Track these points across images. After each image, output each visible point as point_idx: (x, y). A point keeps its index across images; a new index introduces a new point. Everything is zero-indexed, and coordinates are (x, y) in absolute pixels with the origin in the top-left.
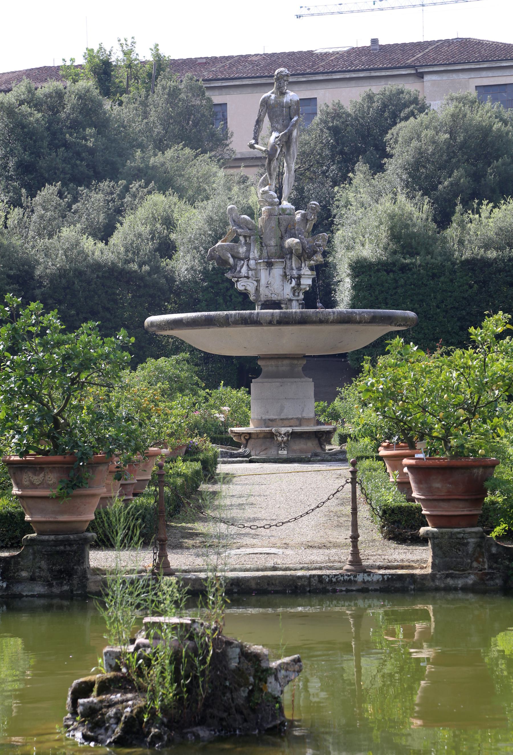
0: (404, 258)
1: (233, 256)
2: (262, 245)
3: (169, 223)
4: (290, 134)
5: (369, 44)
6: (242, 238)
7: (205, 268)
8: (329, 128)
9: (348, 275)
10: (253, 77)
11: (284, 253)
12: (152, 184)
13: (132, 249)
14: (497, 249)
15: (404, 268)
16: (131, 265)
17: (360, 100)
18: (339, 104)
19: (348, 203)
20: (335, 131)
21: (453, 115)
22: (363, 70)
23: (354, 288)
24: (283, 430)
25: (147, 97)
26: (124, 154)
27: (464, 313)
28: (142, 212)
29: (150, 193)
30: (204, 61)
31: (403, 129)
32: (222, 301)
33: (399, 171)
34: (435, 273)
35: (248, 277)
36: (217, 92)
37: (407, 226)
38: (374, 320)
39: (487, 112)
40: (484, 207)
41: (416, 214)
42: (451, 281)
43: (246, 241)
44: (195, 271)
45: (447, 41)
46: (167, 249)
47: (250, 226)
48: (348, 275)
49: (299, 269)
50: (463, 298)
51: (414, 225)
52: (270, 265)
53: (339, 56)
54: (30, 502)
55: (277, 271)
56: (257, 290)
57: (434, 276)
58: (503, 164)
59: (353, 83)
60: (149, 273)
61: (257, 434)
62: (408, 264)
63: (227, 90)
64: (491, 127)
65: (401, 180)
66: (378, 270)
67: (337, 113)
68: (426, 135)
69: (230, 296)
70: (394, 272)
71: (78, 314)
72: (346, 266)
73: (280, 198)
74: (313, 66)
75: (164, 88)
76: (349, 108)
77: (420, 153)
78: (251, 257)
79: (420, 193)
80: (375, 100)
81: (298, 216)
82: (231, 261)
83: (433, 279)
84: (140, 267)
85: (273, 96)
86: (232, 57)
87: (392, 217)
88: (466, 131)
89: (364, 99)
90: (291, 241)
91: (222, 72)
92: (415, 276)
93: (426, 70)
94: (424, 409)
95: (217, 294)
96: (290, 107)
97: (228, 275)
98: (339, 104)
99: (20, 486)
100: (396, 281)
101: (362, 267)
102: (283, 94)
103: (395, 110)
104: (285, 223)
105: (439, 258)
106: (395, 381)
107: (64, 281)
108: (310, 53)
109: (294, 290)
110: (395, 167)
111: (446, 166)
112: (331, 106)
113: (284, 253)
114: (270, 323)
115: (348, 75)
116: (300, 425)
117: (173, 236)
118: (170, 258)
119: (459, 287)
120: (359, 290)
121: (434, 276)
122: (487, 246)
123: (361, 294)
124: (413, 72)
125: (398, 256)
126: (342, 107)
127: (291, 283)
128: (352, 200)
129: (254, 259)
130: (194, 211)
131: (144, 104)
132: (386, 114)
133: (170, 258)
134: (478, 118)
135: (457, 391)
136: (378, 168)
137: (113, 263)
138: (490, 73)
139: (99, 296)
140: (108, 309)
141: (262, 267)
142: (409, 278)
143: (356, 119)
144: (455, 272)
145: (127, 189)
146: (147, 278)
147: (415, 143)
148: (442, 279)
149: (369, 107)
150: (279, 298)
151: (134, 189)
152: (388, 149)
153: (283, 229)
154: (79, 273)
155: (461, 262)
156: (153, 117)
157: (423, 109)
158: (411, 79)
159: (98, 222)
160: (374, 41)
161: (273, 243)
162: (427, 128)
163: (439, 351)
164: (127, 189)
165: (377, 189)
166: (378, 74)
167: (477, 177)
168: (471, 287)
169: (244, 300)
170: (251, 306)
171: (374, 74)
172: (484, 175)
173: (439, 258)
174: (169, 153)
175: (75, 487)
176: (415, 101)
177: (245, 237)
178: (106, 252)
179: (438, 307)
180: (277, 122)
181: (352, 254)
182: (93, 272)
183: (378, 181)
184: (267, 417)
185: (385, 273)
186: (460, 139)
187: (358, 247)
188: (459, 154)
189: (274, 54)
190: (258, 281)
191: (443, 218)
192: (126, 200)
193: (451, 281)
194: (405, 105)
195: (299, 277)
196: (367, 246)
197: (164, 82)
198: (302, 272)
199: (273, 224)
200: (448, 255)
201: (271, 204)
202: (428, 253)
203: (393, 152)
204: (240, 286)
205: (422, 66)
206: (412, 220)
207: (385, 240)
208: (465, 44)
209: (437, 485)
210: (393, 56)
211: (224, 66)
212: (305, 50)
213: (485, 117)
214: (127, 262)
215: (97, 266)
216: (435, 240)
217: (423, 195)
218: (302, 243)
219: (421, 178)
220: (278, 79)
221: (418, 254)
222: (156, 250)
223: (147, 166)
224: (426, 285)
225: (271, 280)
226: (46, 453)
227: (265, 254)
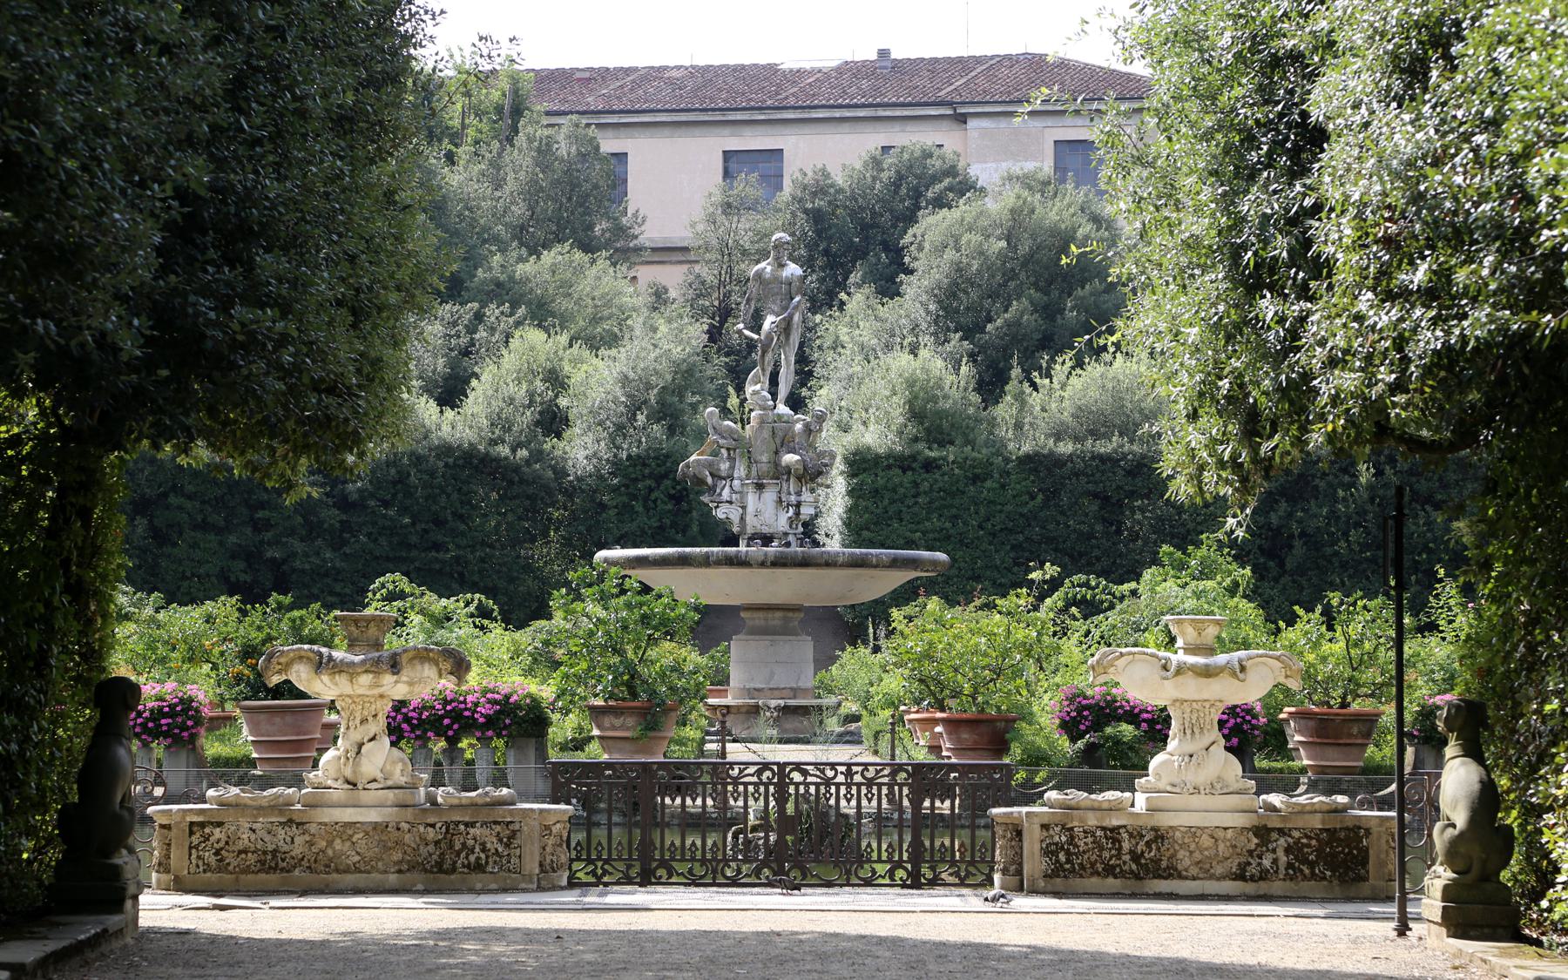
0: (930, 449)
2: (751, 461)
3: (556, 380)
4: (791, 317)
5: (873, 56)
6: (724, 451)
7: (615, 456)
8: (806, 211)
9: (842, 473)
10: (674, 111)
11: (780, 473)
12: (522, 311)
13: (501, 423)
14: (1077, 439)
15: (929, 465)
16: (500, 448)
17: (858, 165)
18: (824, 170)
19: (837, 345)
20: (816, 217)
21: (1012, 211)
22: (864, 106)
23: (850, 493)
24: (773, 703)
25: (500, 155)
26: (473, 260)
27: (1021, 538)
28: (510, 360)
29: (518, 324)
30: (587, 75)
31: (931, 226)
32: (641, 509)
33: (924, 298)
35: (730, 502)
36: (610, 133)
37: (935, 399)
38: (895, 563)
39: (1069, 206)
40: (1058, 367)
41: (950, 378)
42: (1003, 486)
44: (600, 459)
45: (1008, 57)
46: (553, 422)
48: (842, 473)
49: (799, 494)
50: (1022, 515)
51: (946, 397)
52: (760, 487)
53: (824, 77)
54: (610, 742)
55: (770, 496)
56: (742, 519)
57: (976, 479)
58: (1092, 294)
59: (846, 127)
60: (528, 462)
61: (738, 707)
62: (935, 459)
63: (629, 131)
64: (1075, 231)
65: (928, 312)
66: (889, 467)
67: (821, 187)
68: (969, 241)
69: (655, 501)
70: (913, 470)
71: (413, 524)
73: (774, 400)
74: (777, 94)
75: (530, 140)
76: (840, 179)
77: (959, 270)
79: (958, 335)
80: (885, 166)
81: (799, 426)
82: (709, 480)
83: (974, 483)
84: (514, 451)
85: (769, 269)
86: (636, 69)
87: (911, 383)
88: (1033, 236)
89: (866, 164)
90: (790, 458)
91: (619, 98)
93: (971, 110)
94: (956, 670)
95: (634, 497)
97: (705, 499)
98: (824, 170)
99: (599, 727)
100: (916, 484)
101: (864, 460)
102: (782, 266)
103: (919, 187)
105: (984, 451)
106: (931, 644)
107: (393, 471)
108: (772, 69)
109: (791, 521)
110: (917, 292)
111: (999, 294)
112: (810, 174)
113: (780, 473)
114: (762, 564)
115: (837, 114)
116: (795, 697)
117: (563, 402)
118: (559, 436)
121: (976, 479)
122: (1058, 437)
124: (950, 112)
125: (921, 446)
126: (827, 176)
128: (845, 338)
130: (595, 361)
131: (496, 164)
132: (903, 191)
133: (559, 436)
134: (1053, 216)
135: (985, 655)
136: (888, 288)
137: (471, 444)
139: (448, 496)
140: (461, 517)
141: (751, 489)
143: (854, 198)
144: (1008, 473)
145: (479, 317)
146: (525, 469)
147: (950, 254)
148: (988, 484)
149: (874, 179)
151: (493, 319)
152: (907, 260)
153: (778, 441)
154: (417, 459)
156: (511, 186)
157: (965, 187)
158: (945, 124)
159: (434, 372)
160: (883, 53)
161: (764, 458)
162: (970, 230)
163: (978, 602)
164: (479, 317)
165: (888, 325)
166: (888, 113)
167: (1050, 312)
168: (1033, 498)
170: (732, 540)
171: (881, 113)
172: (1061, 311)
173: (984, 451)
174: (548, 257)
175: (653, 729)
176: (951, 171)
178: (460, 427)
179: (981, 527)
181: (848, 440)
182: (438, 457)
183: (890, 311)
184: (752, 685)
185: (900, 472)
186: (1024, 248)
187: (857, 426)
188: (1023, 276)
189: (707, 68)
190: (744, 508)
191: (991, 385)
192: (477, 336)
193: (1003, 486)
194: (935, 179)
195: (798, 505)
196: (871, 428)
197: (530, 130)
198: (803, 498)
199: (766, 434)
200: (999, 447)
201: (764, 408)
202: (968, 442)
203: (915, 265)
204: (720, 514)
206: (942, 389)
207: (901, 420)
209: (965, 736)
210: (916, 81)
211: (621, 87)
212: (763, 61)
213: (1066, 214)
214: (494, 442)
215: (446, 450)
216: (978, 421)
217: (961, 339)
218: (804, 461)
219: (959, 313)
220: (775, 247)
221: (952, 443)
222: (537, 423)
223: (511, 278)
225: (761, 506)
226: (624, 699)
227: (754, 473)
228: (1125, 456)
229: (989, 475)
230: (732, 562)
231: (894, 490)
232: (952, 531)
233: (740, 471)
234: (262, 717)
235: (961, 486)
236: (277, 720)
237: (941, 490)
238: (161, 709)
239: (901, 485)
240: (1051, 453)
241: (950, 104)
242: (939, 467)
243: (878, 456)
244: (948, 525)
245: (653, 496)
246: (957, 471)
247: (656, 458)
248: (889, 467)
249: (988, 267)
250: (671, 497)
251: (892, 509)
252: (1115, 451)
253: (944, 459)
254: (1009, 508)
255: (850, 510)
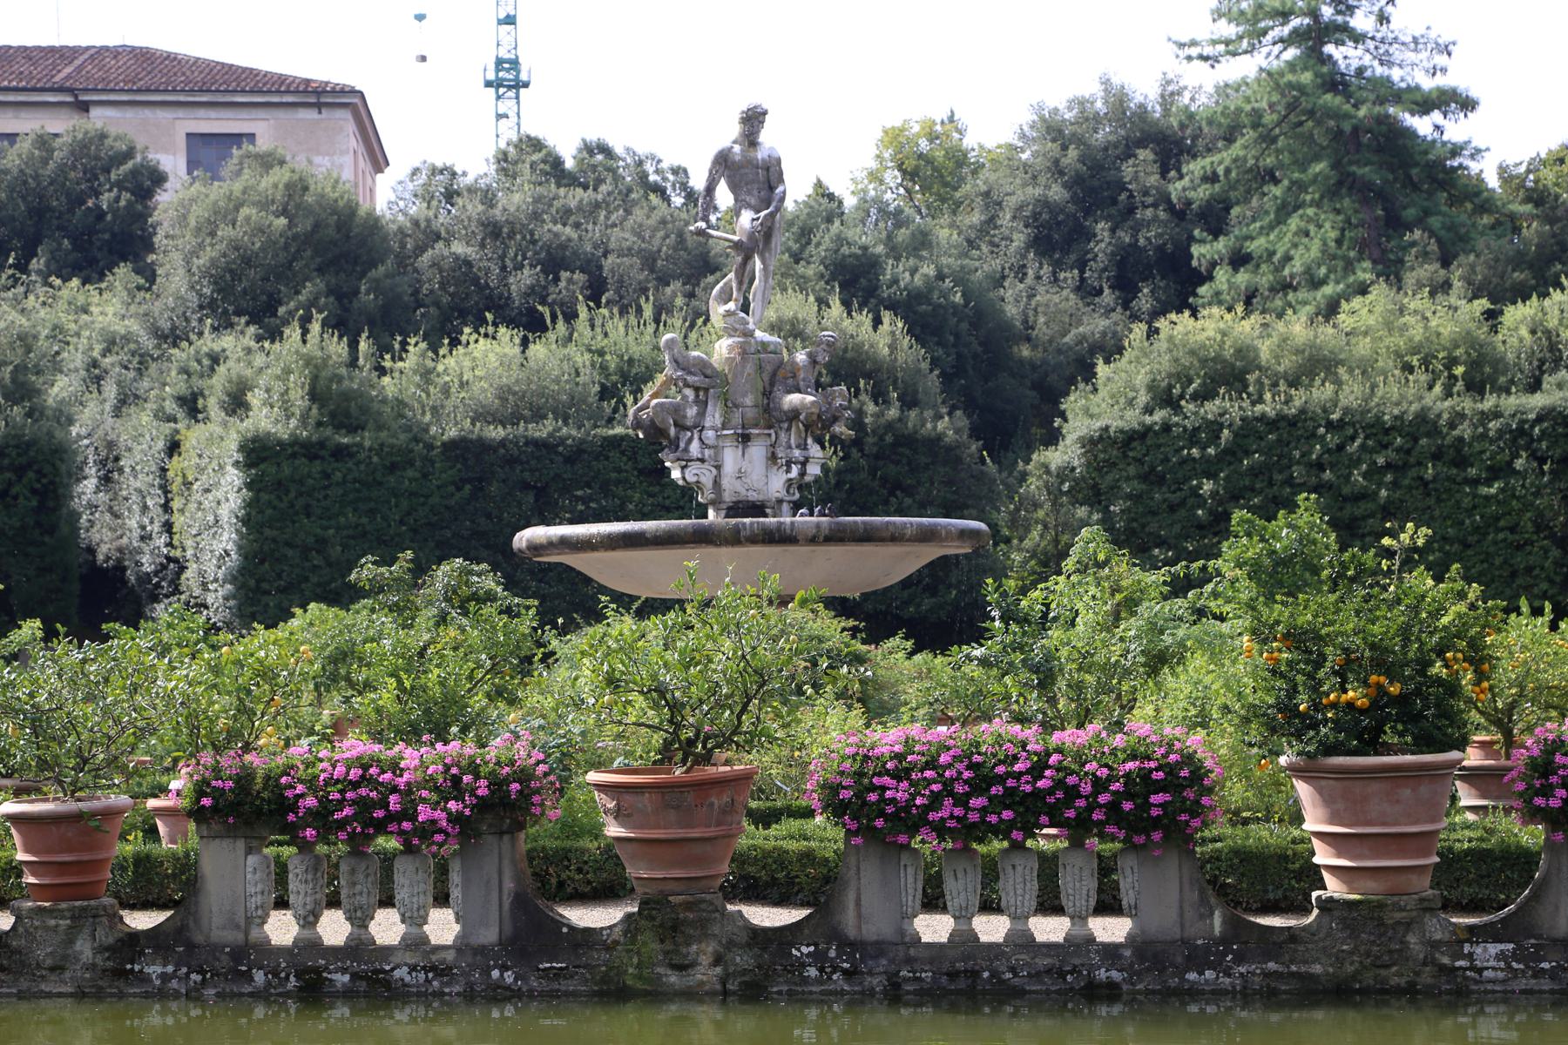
1: (676, 425)
2: (729, 405)
15: (340, 453)
34: (396, 461)
35: (702, 460)
42: (425, 476)
43: (697, 396)
47: (709, 372)
50: (447, 507)
52: (745, 439)
55: (758, 451)
56: (717, 483)
57: (393, 468)
62: (347, 446)
66: (294, 456)
70: (323, 458)
72: (234, 446)
78: (707, 424)
79: (243, 320)
82: (672, 431)
86: (75, 51)
92: (362, 467)
93: (95, 98)
96: (768, 169)
100: (327, 476)
101: (264, 448)
104: (769, 368)
114: (813, 540)
119: (439, 487)
120: (259, 490)
123: (265, 497)
124: (69, 99)
127: (788, 471)
129: (712, 428)
138: (212, 113)
142: (350, 470)
150: (761, 498)
153: (766, 377)
155: (444, 444)
161: (749, 401)
169: (683, 501)
172: (356, 292)
177: (697, 389)
179: (402, 522)
180: (749, 193)
190: (718, 467)
193: (425, 476)
199: (750, 368)
205: (86, 90)
208: (144, 56)
224: (380, 484)
225: (745, 466)
228: (562, 440)
229: (411, 463)
230: (704, 537)
231: (301, 482)
232: (368, 528)
233: (714, 417)
234: (1375, 787)
235: (379, 476)
236: (1406, 793)
237: (355, 481)
238: (1145, 775)
239: (309, 476)
240: (480, 439)
241: (70, 91)
242: (351, 455)
243: (280, 443)
244: (364, 520)
245: (14, 491)
246: (375, 459)
247: (17, 447)
248: (294, 456)
249: (270, 244)
250: (34, 491)
251: (300, 502)
252: (550, 435)
253: (359, 445)
254: (435, 500)
255: (248, 505)
